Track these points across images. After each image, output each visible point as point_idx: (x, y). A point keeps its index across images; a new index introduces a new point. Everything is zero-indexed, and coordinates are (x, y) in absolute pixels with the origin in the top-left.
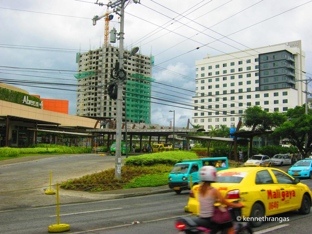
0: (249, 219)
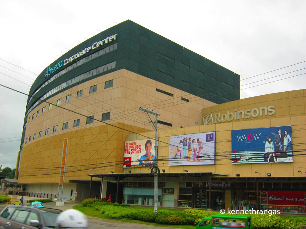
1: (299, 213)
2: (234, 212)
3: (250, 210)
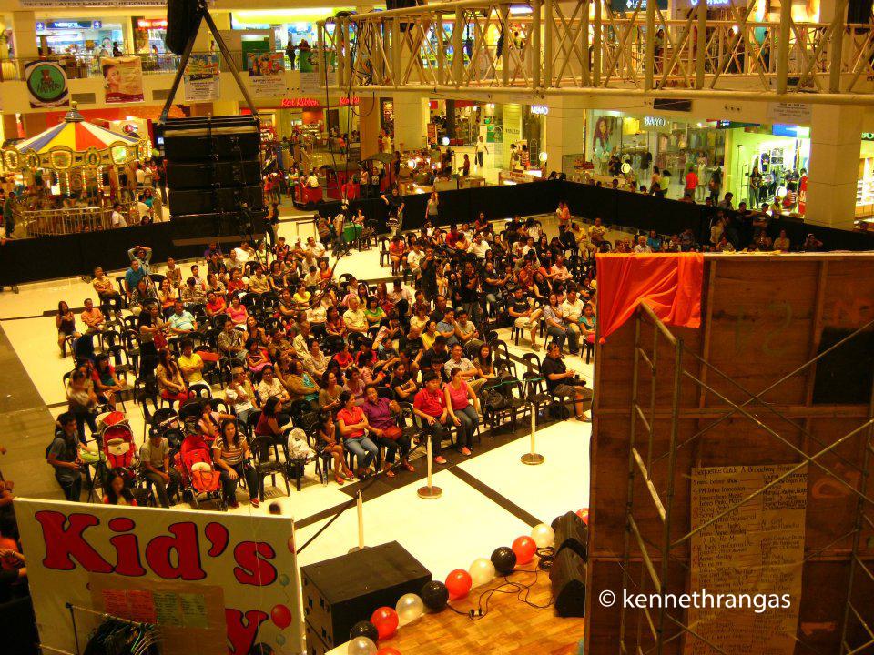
0: (646, 600)
1: (274, 452)
2: (646, 600)
3: (695, 595)
